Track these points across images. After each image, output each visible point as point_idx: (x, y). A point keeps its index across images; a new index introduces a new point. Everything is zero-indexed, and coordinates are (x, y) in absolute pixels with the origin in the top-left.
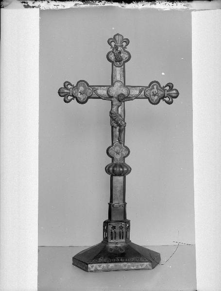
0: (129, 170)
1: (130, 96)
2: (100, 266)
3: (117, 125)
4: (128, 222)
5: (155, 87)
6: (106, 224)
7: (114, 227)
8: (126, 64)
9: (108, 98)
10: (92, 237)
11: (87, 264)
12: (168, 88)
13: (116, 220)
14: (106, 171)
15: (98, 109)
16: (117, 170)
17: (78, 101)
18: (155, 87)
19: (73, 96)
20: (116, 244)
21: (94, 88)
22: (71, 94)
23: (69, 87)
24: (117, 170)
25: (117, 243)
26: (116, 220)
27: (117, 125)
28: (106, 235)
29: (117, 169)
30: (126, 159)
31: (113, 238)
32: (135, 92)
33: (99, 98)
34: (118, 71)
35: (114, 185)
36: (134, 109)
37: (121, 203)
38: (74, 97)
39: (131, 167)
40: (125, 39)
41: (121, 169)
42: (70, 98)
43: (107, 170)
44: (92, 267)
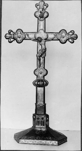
0: (47, 84)
1: (48, 39)
2: (51, 142)
3: (42, 55)
4: (47, 116)
5: (19, 32)
6: (34, 115)
7: (43, 119)
8: (46, 19)
9: (35, 39)
10: (28, 124)
11: (58, 141)
12: (71, 33)
13: (41, 113)
14: (33, 84)
15: (32, 47)
16: (41, 83)
17: (61, 42)
18: (19, 32)
19: (14, 38)
20: (41, 128)
21: (27, 34)
22: (13, 37)
23: (12, 33)
24: (41, 83)
25: (41, 128)
26: (41, 113)
27: (42, 55)
28: (47, 123)
29: (41, 83)
30: (45, 77)
31: (38, 125)
32: (51, 36)
33: (30, 39)
34: (42, 23)
35: (38, 92)
36: (53, 47)
37: (42, 103)
38: (15, 39)
39: (47, 80)
40: (46, 4)
41: (39, 83)
42: (12, 40)
43: (34, 84)
44: (22, 141)
